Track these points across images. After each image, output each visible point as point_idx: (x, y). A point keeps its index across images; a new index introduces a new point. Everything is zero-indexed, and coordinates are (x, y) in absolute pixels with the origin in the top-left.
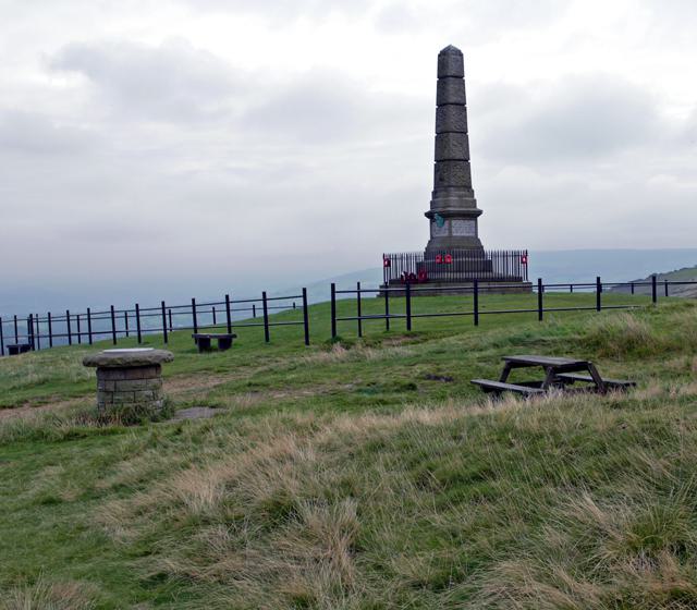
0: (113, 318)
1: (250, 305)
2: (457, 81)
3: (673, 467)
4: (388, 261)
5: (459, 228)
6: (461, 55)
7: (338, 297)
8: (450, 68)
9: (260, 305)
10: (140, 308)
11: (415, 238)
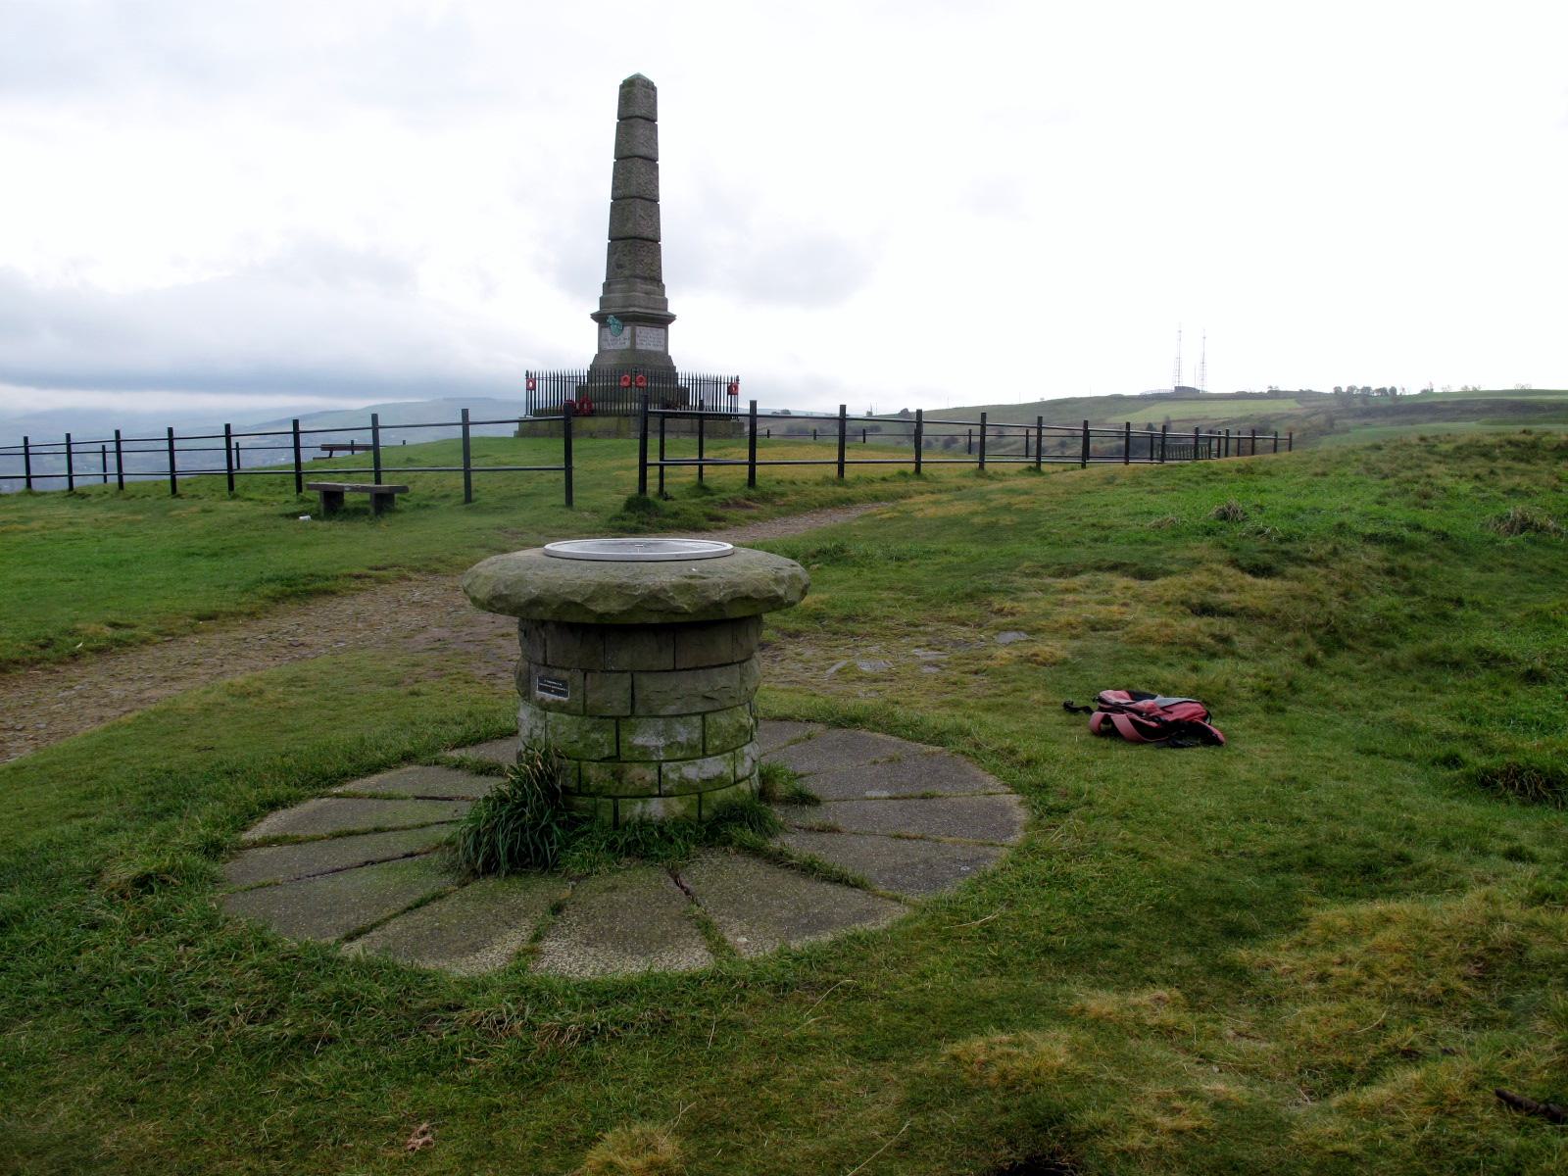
0: (69, 453)
1: (965, 429)
2: (648, 125)
3: (914, 705)
4: (531, 380)
5: (646, 339)
6: (654, 89)
7: (475, 432)
8: (637, 105)
9: (977, 429)
10: (30, 442)
11: (572, 344)
